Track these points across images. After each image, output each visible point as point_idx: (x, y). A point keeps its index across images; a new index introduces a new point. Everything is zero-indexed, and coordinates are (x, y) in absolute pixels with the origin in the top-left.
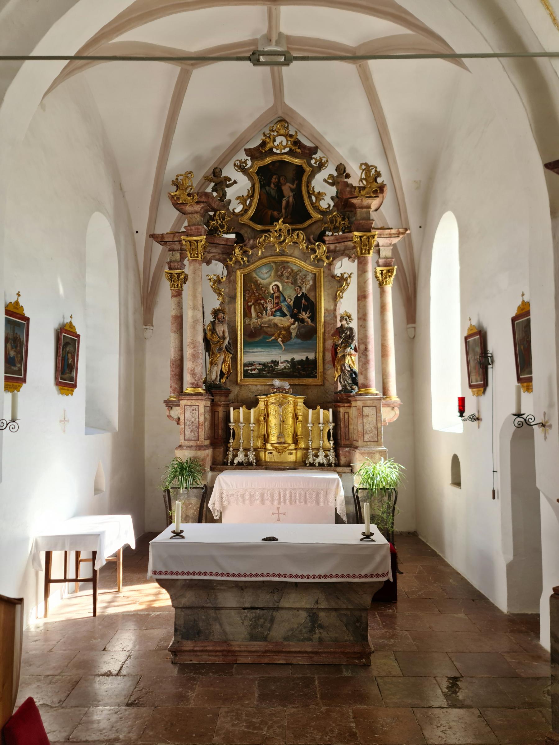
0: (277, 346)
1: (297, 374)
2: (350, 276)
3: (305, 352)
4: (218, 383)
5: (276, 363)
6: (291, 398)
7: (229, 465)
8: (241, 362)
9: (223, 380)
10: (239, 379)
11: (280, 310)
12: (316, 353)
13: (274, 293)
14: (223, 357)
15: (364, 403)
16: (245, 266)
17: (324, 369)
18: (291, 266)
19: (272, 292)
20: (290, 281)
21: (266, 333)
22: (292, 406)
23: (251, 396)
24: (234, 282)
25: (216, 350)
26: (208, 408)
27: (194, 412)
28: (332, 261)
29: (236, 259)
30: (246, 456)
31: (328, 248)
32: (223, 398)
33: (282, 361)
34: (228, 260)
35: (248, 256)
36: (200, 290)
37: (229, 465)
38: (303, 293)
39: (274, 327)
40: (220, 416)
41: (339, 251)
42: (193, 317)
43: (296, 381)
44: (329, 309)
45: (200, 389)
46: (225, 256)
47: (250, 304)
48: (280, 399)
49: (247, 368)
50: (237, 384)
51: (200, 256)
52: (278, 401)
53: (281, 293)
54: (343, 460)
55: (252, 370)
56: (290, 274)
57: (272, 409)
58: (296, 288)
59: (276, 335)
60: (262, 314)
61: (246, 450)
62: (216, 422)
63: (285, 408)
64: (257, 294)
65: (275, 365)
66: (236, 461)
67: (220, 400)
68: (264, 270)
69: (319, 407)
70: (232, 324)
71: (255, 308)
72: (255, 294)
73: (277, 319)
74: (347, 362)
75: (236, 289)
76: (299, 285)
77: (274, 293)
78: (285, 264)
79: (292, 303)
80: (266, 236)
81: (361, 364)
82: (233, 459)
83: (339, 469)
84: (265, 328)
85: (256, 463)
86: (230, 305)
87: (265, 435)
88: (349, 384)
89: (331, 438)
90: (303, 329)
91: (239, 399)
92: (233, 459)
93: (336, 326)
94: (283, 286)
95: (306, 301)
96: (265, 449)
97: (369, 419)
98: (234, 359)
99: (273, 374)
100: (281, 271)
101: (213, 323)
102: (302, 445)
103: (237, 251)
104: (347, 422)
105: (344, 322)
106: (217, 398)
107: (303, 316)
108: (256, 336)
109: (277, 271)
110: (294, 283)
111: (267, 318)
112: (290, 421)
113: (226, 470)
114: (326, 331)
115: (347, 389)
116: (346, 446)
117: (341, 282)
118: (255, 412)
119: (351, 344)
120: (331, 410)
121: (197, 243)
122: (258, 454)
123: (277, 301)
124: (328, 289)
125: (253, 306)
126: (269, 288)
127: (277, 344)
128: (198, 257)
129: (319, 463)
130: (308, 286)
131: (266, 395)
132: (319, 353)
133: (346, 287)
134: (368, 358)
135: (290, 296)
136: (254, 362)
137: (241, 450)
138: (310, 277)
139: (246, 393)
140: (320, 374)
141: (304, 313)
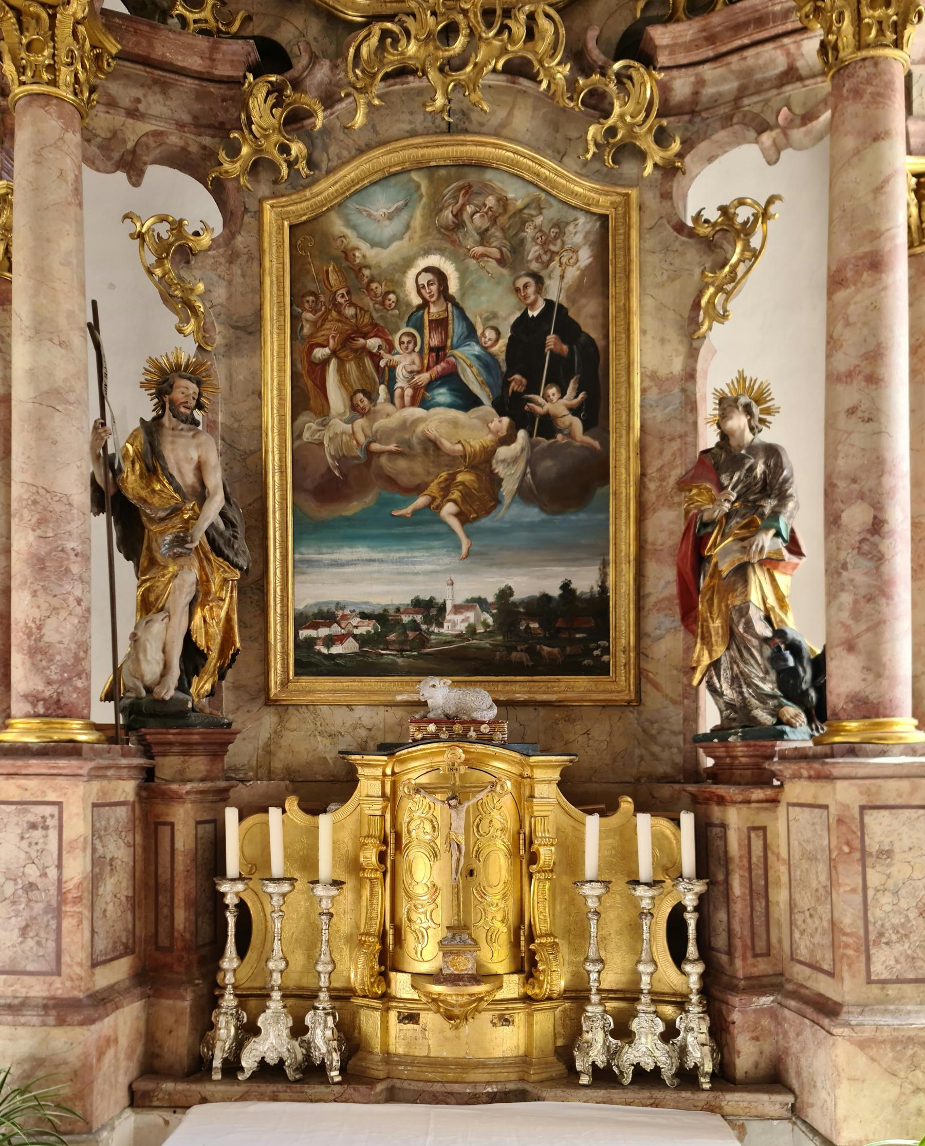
0: (436, 536)
1: (524, 657)
2: (765, 215)
3: (559, 561)
4: (169, 691)
5: (431, 610)
6: (502, 764)
7: (217, 1076)
8: (285, 605)
9: (202, 685)
10: (275, 678)
11: (451, 379)
12: (605, 564)
13: (425, 304)
14: (191, 576)
15: (868, 792)
16: (297, 184)
17: (640, 635)
18: (498, 184)
19: (416, 301)
20: (494, 252)
21: (391, 482)
22: (507, 803)
23: (327, 749)
24: (251, 258)
25: (162, 540)
26: (122, 813)
27: (38, 834)
28: (680, 155)
29: (258, 150)
30: (299, 1030)
31: (664, 88)
32: (198, 765)
33: (460, 600)
34: (222, 155)
35: (309, 138)
36: (66, 243)
37: (217, 1076)
38: (549, 304)
39: (425, 451)
40: (179, 845)
41: (715, 102)
42: (32, 374)
43: (520, 688)
44: (663, 372)
45: (75, 724)
46: (207, 141)
47: (320, 353)
48: (452, 768)
49: (312, 633)
50: (269, 702)
51: (65, 75)
52: (445, 777)
53: (456, 305)
54: (747, 1055)
55: (330, 641)
56: (494, 220)
57: (421, 817)
58: (520, 283)
59: (433, 488)
60: (371, 396)
61: (301, 999)
62: (164, 875)
63: (479, 813)
64: (350, 311)
65: (428, 620)
66: (249, 1062)
67: (184, 771)
68: (382, 203)
69: (627, 804)
70: (244, 443)
71: (341, 370)
72: (340, 312)
73: (440, 422)
74: (755, 597)
75: (259, 289)
76: (534, 266)
77: (425, 304)
78: (473, 176)
79: (500, 348)
80: (385, 34)
81: (846, 598)
82: (239, 1045)
83: (734, 1100)
84: (383, 460)
85: (342, 1070)
86: (236, 361)
87: (383, 937)
88: (763, 697)
89: (692, 950)
90: (548, 463)
91: (278, 765)
92: (239, 1045)
93: (695, 445)
94: (463, 274)
95: (564, 340)
96: (386, 997)
97: (894, 870)
98: (253, 591)
99: (422, 656)
100: (454, 195)
101: (152, 430)
102: (557, 979)
103: (260, 107)
104: (758, 872)
105: (738, 422)
106: (168, 765)
107: (548, 406)
108: (345, 494)
109: (435, 209)
110: (513, 257)
111: (392, 416)
112: (498, 867)
113: (204, 1100)
114: (651, 470)
115: (754, 721)
116: (758, 986)
117: (723, 241)
118: (337, 827)
119: (775, 515)
120: (687, 820)
121: (53, 17)
122: (355, 1015)
123: (435, 342)
124: (662, 286)
125: (333, 364)
126: (402, 284)
127: (436, 528)
128: (54, 83)
129: (638, 1070)
130: (572, 273)
131: (388, 749)
132: (621, 563)
133: (741, 270)
134: (885, 568)
135: (495, 316)
136: (339, 606)
137: (275, 1003)
138: (580, 231)
139: (305, 745)
140: (622, 659)
141: (553, 391)
